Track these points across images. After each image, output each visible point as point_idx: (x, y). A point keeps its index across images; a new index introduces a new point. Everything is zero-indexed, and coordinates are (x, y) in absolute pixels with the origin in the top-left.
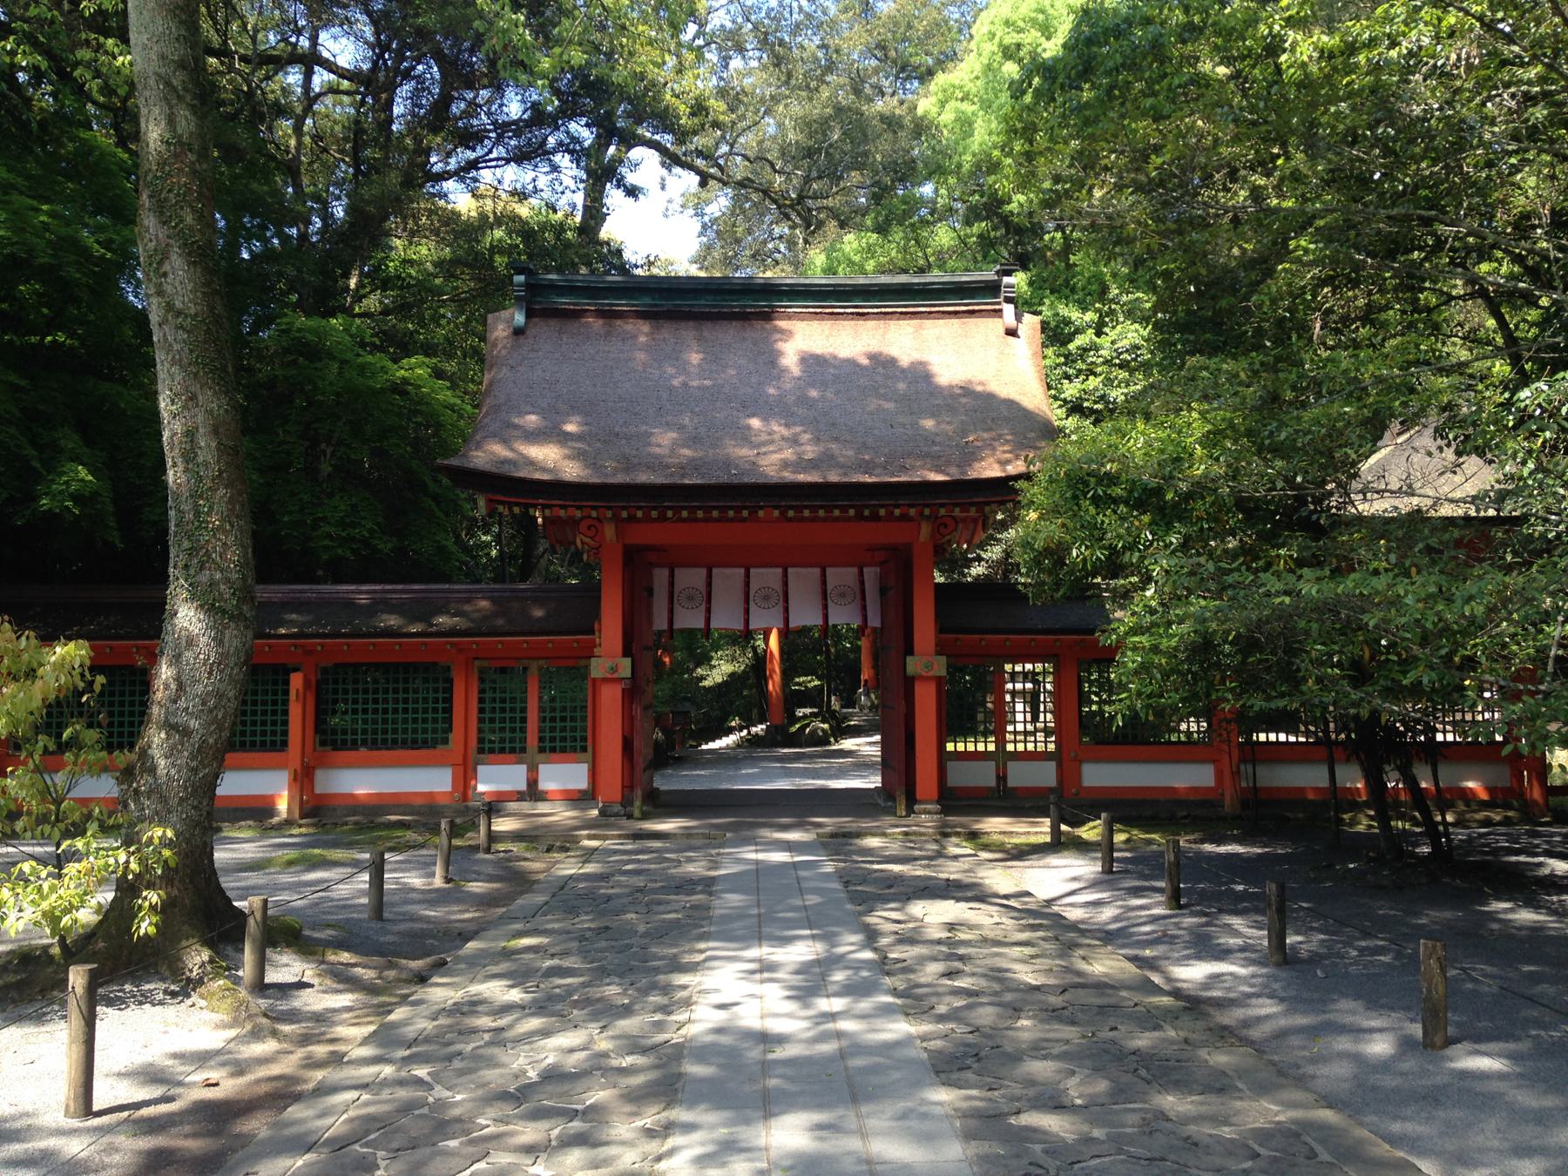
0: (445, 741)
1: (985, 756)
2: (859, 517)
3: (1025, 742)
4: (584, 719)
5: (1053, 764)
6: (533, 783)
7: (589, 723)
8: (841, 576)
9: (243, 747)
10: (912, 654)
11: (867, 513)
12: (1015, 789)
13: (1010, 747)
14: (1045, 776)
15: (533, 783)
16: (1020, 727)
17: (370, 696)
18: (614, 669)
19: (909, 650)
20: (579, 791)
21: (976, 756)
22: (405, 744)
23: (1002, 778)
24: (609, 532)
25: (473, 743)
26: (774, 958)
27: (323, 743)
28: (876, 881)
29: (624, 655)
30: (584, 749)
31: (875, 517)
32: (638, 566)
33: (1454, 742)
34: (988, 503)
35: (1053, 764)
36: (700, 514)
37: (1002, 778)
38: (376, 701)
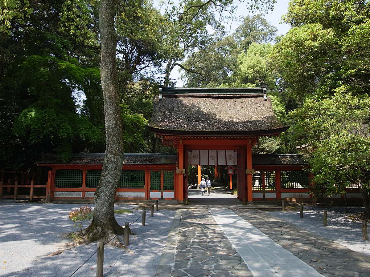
0: (143, 187)
1: (260, 191)
2: (231, 139)
3: (258, 188)
4: (173, 183)
5: (275, 193)
6: (162, 196)
7: (174, 184)
8: (230, 153)
9: (121, 187)
10: (247, 169)
11: (232, 138)
12: (267, 199)
13: (266, 190)
14: (274, 196)
15: (162, 196)
16: (257, 185)
17: (70, 174)
18: (182, 172)
19: (246, 168)
20: (172, 198)
21: (258, 191)
22: (135, 188)
23: (264, 196)
24: (181, 141)
25: (149, 188)
26: (250, 236)
27: (87, 186)
28: (67, 208)
29: (184, 169)
30: (173, 189)
31: (234, 139)
32: (187, 149)
33: (302, 188)
34: (259, 136)
35: (275, 193)
36: (186, 138)
37: (264, 196)
38: (75, 175)
